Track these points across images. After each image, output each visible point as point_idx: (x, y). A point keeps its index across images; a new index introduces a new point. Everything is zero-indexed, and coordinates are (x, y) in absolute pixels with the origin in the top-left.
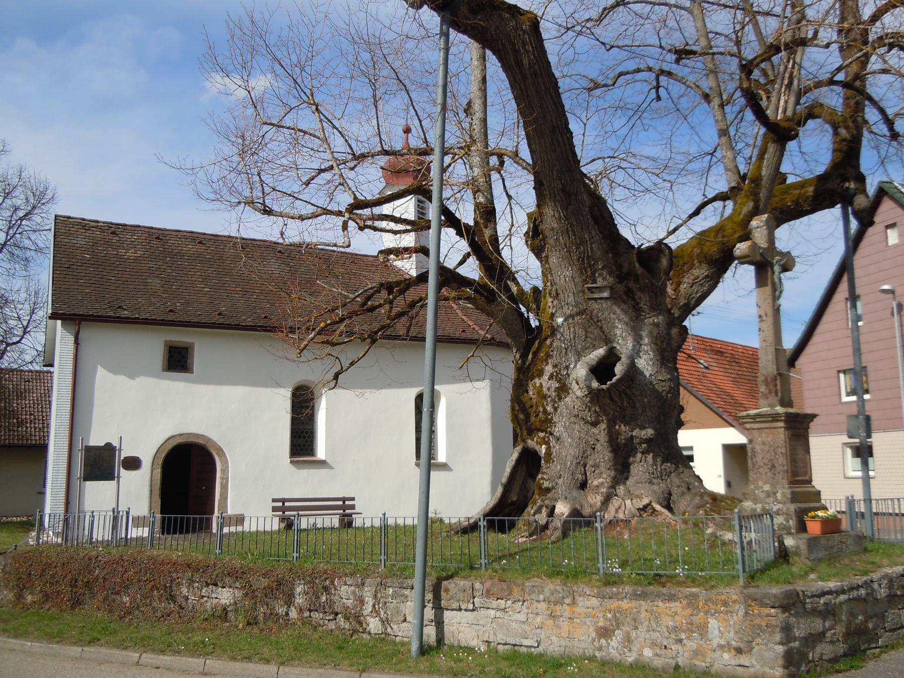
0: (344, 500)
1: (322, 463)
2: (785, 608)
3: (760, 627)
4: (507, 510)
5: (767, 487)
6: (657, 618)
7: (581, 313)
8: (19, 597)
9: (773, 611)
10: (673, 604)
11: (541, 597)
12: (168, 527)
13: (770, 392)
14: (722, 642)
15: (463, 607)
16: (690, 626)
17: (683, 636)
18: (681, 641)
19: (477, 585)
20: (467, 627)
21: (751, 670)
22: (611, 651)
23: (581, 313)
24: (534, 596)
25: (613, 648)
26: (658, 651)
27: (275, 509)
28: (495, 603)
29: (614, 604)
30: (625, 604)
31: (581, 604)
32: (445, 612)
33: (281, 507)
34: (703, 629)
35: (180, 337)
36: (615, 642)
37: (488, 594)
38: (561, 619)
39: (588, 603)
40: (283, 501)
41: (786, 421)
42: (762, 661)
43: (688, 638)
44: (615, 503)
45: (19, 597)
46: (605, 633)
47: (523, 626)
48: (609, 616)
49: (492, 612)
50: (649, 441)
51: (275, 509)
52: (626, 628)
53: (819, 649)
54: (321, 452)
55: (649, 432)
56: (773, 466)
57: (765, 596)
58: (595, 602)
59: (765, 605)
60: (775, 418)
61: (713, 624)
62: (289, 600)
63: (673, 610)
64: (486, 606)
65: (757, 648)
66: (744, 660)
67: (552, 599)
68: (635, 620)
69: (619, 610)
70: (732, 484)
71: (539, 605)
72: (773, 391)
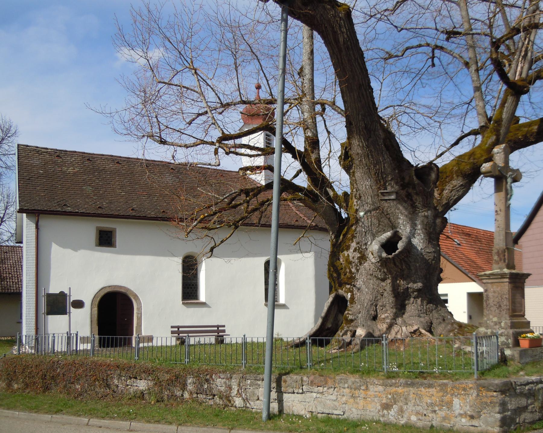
0: (218, 327)
1: (203, 304)
2: (503, 392)
3: (486, 403)
4: (324, 333)
5: (495, 319)
6: (420, 398)
7: (376, 209)
8: (9, 385)
9: (495, 393)
10: (431, 390)
11: (346, 385)
12: (103, 343)
13: (501, 260)
14: (462, 412)
15: (296, 391)
16: (441, 403)
17: (437, 408)
18: (435, 411)
19: (305, 378)
20: (297, 403)
21: (479, 428)
22: (390, 417)
23: (376, 209)
24: (341, 385)
25: (392, 415)
26: (420, 417)
27: (173, 332)
28: (316, 389)
29: (393, 389)
30: (400, 390)
31: (371, 390)
32: (284, 394)
33: (177, 331)
34: (450, 405)
35: (106, 224)
36: (392, 412)
37: (312, 383)
38: (359, 399)
39: (376, 389)
40: (178, 327)
41: (510, 278)
42: (487, 423)
43: (440, 410)
44: (395, 328)
45: (9, 385)
46: (387, 407)
47: (334, 403)
48: (390, 396)
49: (314, 395)
50: (419, 290)
51: (173, 332)
52: (400, 404)
53: (523, 416)
54: (202, 297)
55: (419, 285)
56: (500, 306)
57: (490, 385)
58: (381, 388)
59: (490, 390)
60: (503, 276)
61: (456, 402)
62: (184, 387)
63: (431, 393)
64: (310, 390)
65: (483, 415)
66: (475, 422)
67: (353, 386)
68: (406, 399)
69: (396, 393)
70: (472, 317)
71: (345, 390)
72: (503, 258)
